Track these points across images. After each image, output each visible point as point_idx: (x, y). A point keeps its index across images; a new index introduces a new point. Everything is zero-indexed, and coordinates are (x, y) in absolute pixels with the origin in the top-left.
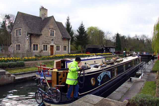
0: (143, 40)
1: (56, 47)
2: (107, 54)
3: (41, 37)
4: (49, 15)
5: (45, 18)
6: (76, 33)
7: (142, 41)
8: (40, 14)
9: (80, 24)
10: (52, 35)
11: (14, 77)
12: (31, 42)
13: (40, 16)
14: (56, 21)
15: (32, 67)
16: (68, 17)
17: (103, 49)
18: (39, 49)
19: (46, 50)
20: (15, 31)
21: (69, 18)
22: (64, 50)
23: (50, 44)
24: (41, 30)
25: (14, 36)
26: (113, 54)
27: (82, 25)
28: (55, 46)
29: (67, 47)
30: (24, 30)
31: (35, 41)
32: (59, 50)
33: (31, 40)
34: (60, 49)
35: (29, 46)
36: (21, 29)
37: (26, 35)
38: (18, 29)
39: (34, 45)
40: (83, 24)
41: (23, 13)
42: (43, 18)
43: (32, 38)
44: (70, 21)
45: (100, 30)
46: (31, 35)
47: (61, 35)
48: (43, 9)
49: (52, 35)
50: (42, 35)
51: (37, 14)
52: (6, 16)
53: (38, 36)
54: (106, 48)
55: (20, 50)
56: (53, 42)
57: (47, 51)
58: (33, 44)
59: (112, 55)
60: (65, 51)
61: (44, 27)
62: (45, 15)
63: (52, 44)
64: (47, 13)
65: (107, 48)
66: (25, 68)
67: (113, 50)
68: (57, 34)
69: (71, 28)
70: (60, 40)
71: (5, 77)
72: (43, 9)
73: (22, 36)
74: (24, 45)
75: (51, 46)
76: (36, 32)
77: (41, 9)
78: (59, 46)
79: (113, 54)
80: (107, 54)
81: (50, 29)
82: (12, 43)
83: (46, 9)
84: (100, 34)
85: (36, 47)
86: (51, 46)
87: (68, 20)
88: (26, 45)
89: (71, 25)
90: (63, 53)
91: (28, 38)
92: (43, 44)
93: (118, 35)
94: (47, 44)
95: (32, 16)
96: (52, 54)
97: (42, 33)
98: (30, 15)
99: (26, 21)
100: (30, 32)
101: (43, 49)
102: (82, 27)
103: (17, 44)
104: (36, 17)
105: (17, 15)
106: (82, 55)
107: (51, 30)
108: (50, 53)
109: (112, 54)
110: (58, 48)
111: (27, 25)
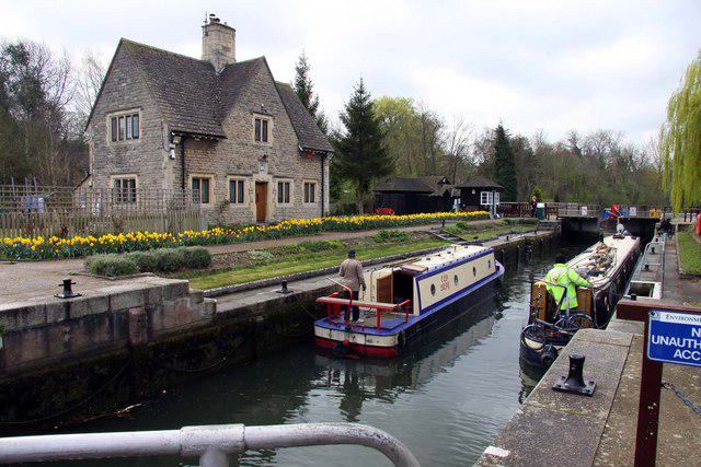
0: (602, 157)
1: (277, 188)
2: (474, 213)
3: (220, 146)
4: (242, 54)
5: (227, 66)
6: (337, 125)
7: (596, 160)
8: (205, 51)
9: (353, 91)
10: (261, 132)
11: (215, 304)
12: (183, 169)
13: (207, 58)
14: (276, 79)
15: (239, 268)
16: (303, 61)
17: (447, 193)
18: (213, 198)
19: (241, 201)
20: (108, 123)
21: (308, 62)
22: (307, 201)
23: (256, 177)
24: (220, 116)
25: (103, 142)
26: (495, 217)
27: (361, 92)
28: (273, 186)
29: (317, 188)
30: (151, 123)
31: (199, 163)
32: (287, 201)
33: (183, 153)
34: (292, 198)
35: (178, 186)
36: (137, 115)
37: (166, 139)
38: (121, 113)
39: (196, 180)
40: (367, 90)
41: (140, 46)
42: (219, 68)
43: (189, 153)
44: (309, 75)
45: (419, 111)
46: (185, 139)
47: (294, 137)
48: (216, 28)
49: (261, 132)
50: (225, 137)
51: (193, 48)
52: (11, 50)
53: (211, 141)
54: (465, 191)
55: (134, 200)
56: (265, 167)
57: (246, 205)
58: (191, 176)
59: (489, 218)
60: (310, 204)
61: (232, 105)
62: (228, 54)
63: (263, 176)
64: (234, 45)
65: (471, 189)
66: (214, 272)
67: (492, 200)
68: (281, 133)
69: (316, 105)
70: (293, 158)
71: (189, 303)
72: (216, 28)
73: (143, 145)
74: (155, 182)
75: (258, 183)
76: (202, 128)
77: (211, 28)
78: (287, 184)
79: (495, 217)
80: (474, 213)
81: (255, 115)
82: (93, 171)
83: (229, 25)
84: (426, 129)
85: (202, 184)
86: (258, 183)
87: (301, 72)
88: (160, 177)
89: (314, 96)
90: (304, 214)
91: (173, 151)
92: (229, 178)
93: (500, 131)
94: (242, 175)
95: (175, 55)
96: (262, 218)
97: (225, 129)
98: (166, 52)
99: (157, 77)
100: (181, 127)
101: (228, 198)
102: (360, 101)
103: (118, 176)
104: (190, 61)
105: (117, 53)
106: (395, 220)
107: (258, 116)
108: (255, 214)
109: (491, 217)
110: (283, 196)
111: (165, 97)
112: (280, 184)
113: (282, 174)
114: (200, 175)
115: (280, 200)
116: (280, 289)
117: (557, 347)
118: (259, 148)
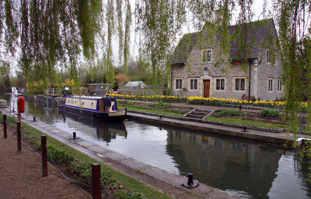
63: (206, 77)
75: (204, 81)
86: (204, 81)
90: (234, 96)
110: (220, 85)
112: (218, 81)
113: (218, 75)
114: (240, 78)
115: (218, 88)
116: (159, 118)
117: (23, 90)
118: (204, 64)
